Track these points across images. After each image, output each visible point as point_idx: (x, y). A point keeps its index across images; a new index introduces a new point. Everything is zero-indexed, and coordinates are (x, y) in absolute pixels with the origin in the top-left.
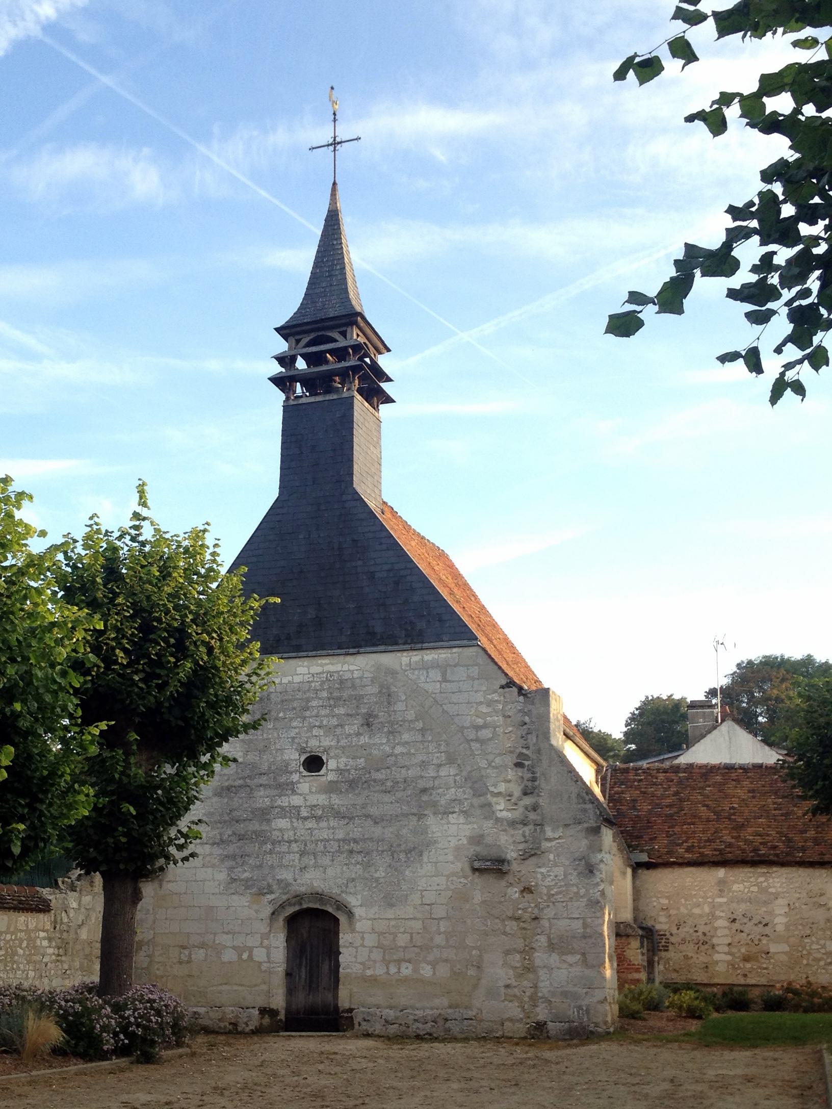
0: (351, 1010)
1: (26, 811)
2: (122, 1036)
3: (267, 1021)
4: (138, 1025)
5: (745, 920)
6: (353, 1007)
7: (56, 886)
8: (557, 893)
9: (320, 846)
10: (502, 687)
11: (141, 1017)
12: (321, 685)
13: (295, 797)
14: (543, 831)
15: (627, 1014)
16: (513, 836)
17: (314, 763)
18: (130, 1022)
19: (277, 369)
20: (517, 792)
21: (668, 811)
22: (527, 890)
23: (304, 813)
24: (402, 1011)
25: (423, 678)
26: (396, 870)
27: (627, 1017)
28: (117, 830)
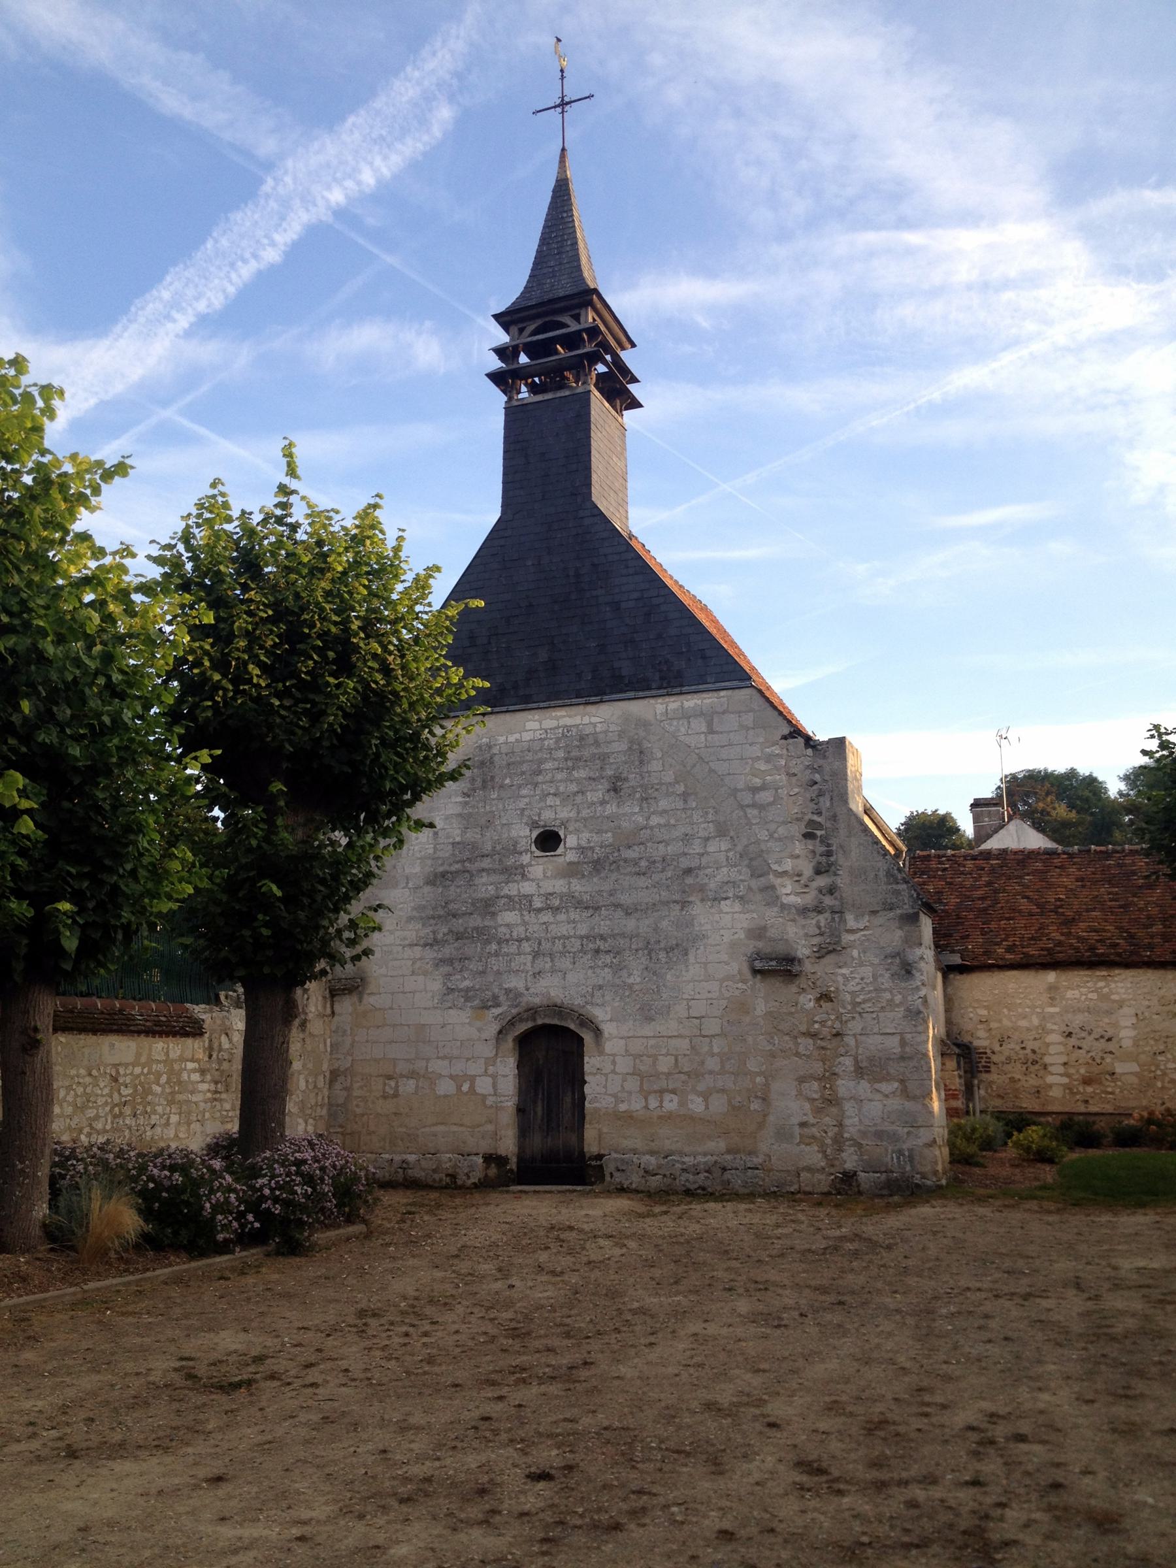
0: (600, 1157)
1: (86, 884)
2: (250, 1217)
3: (493, 1171)
4: (276, 1200)
5: (1084, 1034)
6: (602, 1152)
7: (217, 1001)
8: (864, 1001)
9: (558, 946)
10: (785, 738)
11: (279, 1187)
12: (556, 742)
13: (526, 884)
14: (843, 921)
15: (960, 1159)
16: (804, 926)
17: (548, 841)
18: (263, 1196)
19: (496, 364)
20: (808, 870)
21: (981, 905)
22: (825, 997)
23: (538, 904)
24: (666, 1157)
25: (683, 730)
26: (655, 973)
27: (959, 1162)
28: (256, 919)
